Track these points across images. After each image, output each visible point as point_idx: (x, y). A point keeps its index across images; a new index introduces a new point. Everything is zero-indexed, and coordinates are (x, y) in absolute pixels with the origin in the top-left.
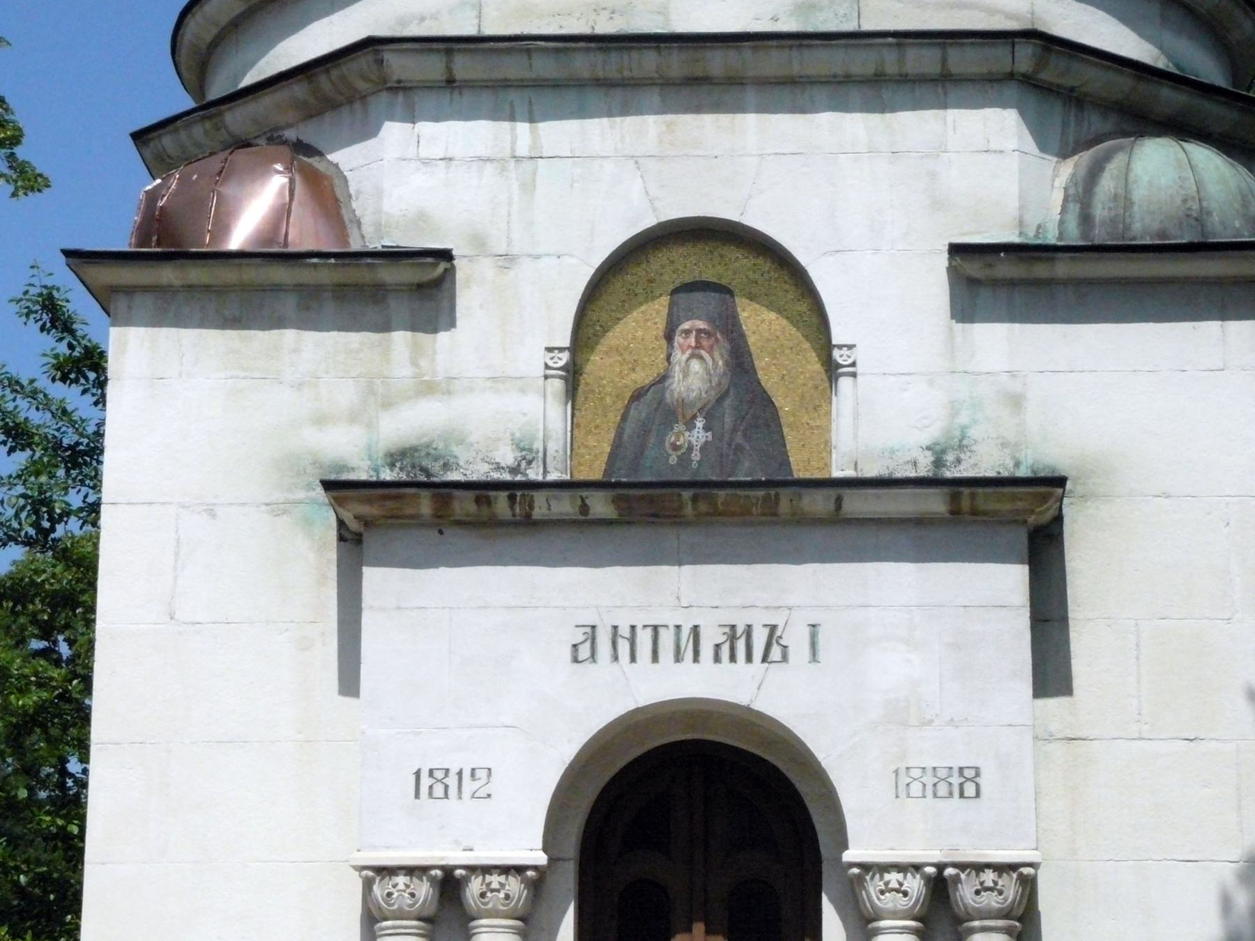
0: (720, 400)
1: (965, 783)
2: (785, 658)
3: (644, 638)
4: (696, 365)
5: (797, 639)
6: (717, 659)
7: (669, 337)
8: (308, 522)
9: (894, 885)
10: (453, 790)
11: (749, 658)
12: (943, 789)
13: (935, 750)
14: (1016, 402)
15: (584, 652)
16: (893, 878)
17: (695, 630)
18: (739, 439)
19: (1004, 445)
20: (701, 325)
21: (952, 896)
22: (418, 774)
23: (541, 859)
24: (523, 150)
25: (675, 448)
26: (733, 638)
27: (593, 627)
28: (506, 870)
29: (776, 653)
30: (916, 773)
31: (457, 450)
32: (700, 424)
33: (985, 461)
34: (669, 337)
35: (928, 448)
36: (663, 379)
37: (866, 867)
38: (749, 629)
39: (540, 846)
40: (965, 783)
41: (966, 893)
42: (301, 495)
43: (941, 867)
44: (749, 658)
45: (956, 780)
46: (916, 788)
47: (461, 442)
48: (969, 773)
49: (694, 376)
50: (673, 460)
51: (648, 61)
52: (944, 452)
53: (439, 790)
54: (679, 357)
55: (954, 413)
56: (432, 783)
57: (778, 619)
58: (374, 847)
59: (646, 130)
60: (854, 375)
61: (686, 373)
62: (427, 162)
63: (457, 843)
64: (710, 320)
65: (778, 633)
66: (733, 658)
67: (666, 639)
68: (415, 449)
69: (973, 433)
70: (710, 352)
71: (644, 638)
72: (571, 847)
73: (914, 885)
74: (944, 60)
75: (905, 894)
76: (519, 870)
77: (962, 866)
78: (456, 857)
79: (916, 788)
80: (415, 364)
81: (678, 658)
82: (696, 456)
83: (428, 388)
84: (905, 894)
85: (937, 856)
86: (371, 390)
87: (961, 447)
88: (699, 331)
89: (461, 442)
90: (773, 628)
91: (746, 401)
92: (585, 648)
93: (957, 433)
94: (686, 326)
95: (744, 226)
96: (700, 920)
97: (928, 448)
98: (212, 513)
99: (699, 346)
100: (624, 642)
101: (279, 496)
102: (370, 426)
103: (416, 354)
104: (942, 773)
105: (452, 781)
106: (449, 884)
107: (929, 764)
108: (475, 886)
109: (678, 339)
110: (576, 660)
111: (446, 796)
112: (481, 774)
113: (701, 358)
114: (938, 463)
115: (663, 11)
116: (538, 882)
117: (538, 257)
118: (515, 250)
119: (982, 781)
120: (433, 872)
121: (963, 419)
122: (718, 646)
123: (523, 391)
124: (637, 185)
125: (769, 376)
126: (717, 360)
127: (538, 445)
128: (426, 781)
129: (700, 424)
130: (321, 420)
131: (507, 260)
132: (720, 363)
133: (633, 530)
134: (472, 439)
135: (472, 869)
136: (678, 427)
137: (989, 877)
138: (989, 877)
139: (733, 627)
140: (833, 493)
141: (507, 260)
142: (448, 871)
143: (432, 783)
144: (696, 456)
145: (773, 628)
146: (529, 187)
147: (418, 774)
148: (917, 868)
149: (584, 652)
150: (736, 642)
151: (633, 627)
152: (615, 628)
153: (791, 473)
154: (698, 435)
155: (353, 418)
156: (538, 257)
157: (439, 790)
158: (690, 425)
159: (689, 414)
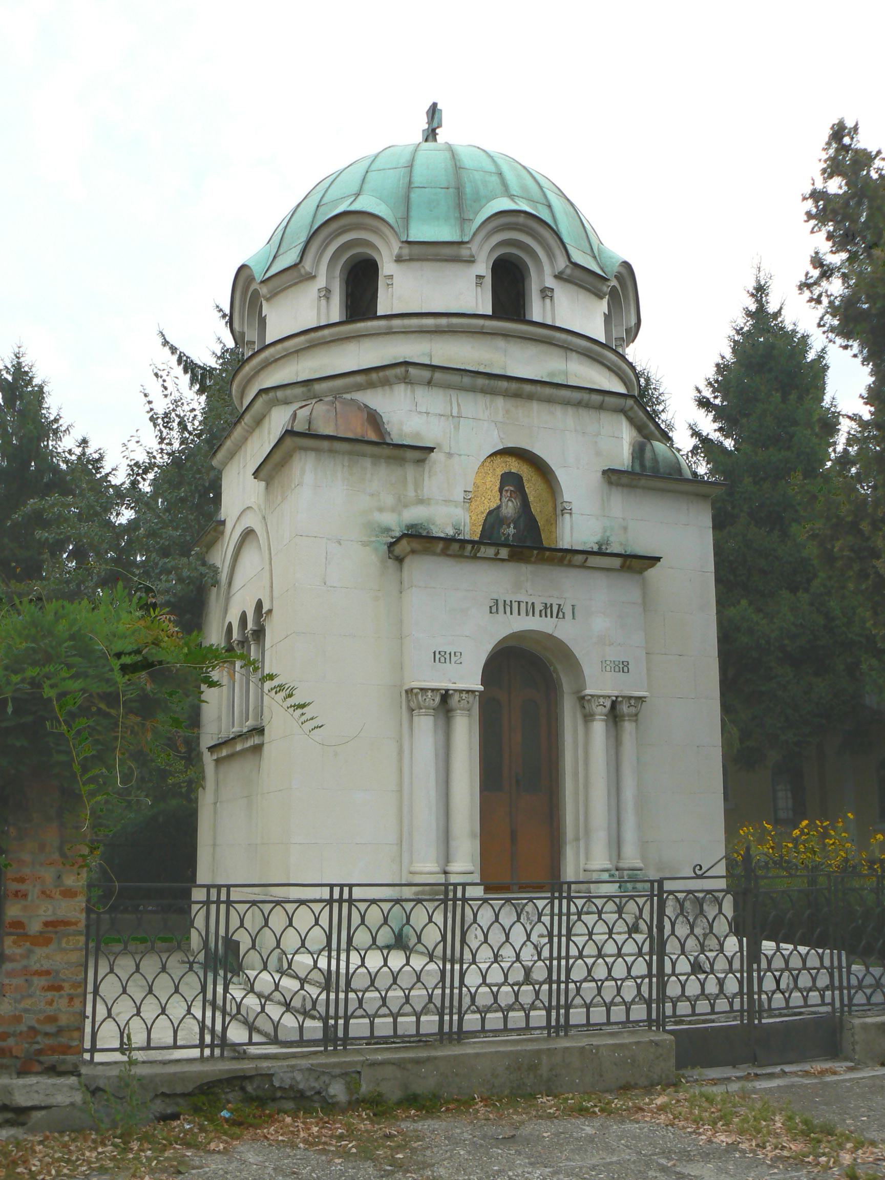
0: (519, 517)
1: (623, 667)
2: (564, 617)
3: (515, 605)
4: (510, 504)
5: (567, 610)
6: (541, 616)
7: (501, 490)
8: (376, 550)
11: (552, 617)
12: (617, 669)
13: (613, 654)
14: (625, 529)
15: (494, 609)
16: (601, 700)
17: (533, 604)
19: (621, 544)
20: (512, 488)
22: (435, 653)
26: (546, 608)
28: (468, 692)
29: (561, 615)
30: (608, 663)
31: (432, 527)
37: (592, 696)
38: (551, 605)
40: (623, 667)
42: (374, 539)
43: (617, 697)
44: (552, 617)
45: (621, 666)
46: (608, 668)
47: (433, 524)
48: (625, 664)
50: (503, 538)
51: (504, 384)
53: (442, 660)
54: (505, 500)
55: (605, 532)
56: (440, 657)
57: (561, 602)
58: (419, 681)
60: (571, 514)
62: (420, 413)
63: (450, 680)
64: (515, 487)
66: (546, 616)
67: (523, 606)
68: (416, 525)
69: (612, 539)
71: (515, 605)
78: (451, 686)
79: (608, 668)
80: (416, 491)
81: (527, 614)
82: (511, 538)
83: (421, 501)
85: (616, 693)
86: (399, 500)
87: (607, 544)
89: (433, 524)
90: (560, 605)
92: (494, 607)
94: (507, 488)
99: (511, 496)
100: (508, 606)
101: (365, 539)
102: (400, 514)
104: (617, 663)
105: (447, 656)
106: (446, 696)
107: (612, 659)
108: (456, 697)
109: (504, 493)
110: (491, 612)
112: (458, 654)
114: (600, 548)
115: (504, 368)
119: (630, 666)
121: (608, 534)
122: (541, 611)
123: (456, 506)
124: (496, 432)
125: (535, 509)
126: (517, 502)
127: (462, 528)
128: (438, 656)
130: (381, 510)
131: (450, 455)
133: (510, 563)
134: (438, 523)
135: (455, 690)
136: (505, 526)
137: (464, 695)
140: (585, 556)
141: (450, 455)
142: (447, 691)
143: (440, 657)
144: (511, 538)
145: (560, 605)
146: (457, 428)
147: (435, 653)
149: (494, 609)
150: (547, 610)
154: (511, 530)
155: (393, 510)
156: (460, 455)
157: (442, 660)
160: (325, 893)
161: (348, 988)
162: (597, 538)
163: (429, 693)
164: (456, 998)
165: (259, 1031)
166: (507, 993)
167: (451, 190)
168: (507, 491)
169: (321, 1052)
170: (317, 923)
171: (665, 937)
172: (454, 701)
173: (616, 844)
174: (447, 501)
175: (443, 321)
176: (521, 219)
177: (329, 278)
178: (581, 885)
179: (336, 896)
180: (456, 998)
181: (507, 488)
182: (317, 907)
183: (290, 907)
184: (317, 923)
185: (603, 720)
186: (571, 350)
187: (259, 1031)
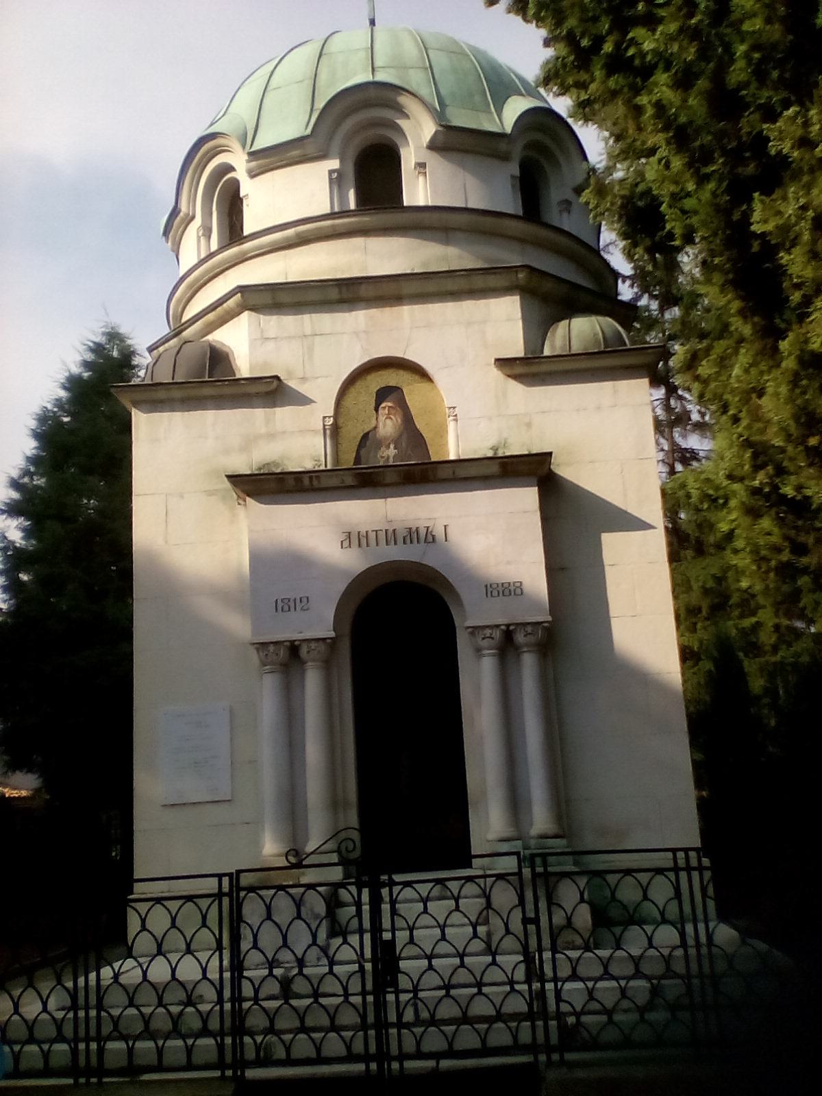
0: (401, 436)
4: (388, 421)
6: (405, 543)
7: (377, 409)
9: (488, 635)
10: (292, 609)
15: (346, 544)
16: (488, 632)
18: (409, 452)
21: (514, 638)
23: (332, 634)
24: (308, 331)
25: (382, 457)
27: (349, 533)
28: (318, 640)
32: (392, 446)
33: (516, 450)
34: (377, 409)
35: (491, 449)
36: (375, 428)
39: (332, 628)
41: (520, 638)
43: (508, 626)
49: (388, 425)
52: (497, 449)
53: (286, 608)
54: (382, 418)
59: (359, 318)
61: (385, 426)
64: (394, 402)
65: (430, 530)
68: (268, 464)
69: (509, 441)
70: (395, 415)
72: (347, 629)
73: (497, 634)
74: (691, 947)
75: (493, 638)
76: (324, 639)
77: (517, 624)
83: (271, 436)
84: (493, 638)
88: (389, 407)
91: (411, 435)
93: (503, 442)
95: (405, 359)
96: (542, 1053)
97: (491, 449)
98: (182, 497)
103: (268, 421)
106: (294, 649)
109: (380, 411)
111: (289, 610)
113: (390, 418)
116: (331, 644)
117: (317, 378)
118: (306, 376)
120: (285, 644)
122: (404, 538)
129: (392, 446)
132: (399, 420)
133: (363, 490)
138: (529, 629)
139: (410, 529)
142: (292, 642)
148: (498, 626)
151: (367, 532)
152: (359, 532)
153: (429, 457)
154: (392, 451)
157: (286, 608)
158: (388, 447)
159: (388, 443)
160: (665, 860)
161: (100, 1007)
162: (492, 442)
163: (272, 648)
164: (93, 1023)
165: (346, 1028)
166: (191, 1013)
167: (306, 82)
168: (384, 408)
169: (69, 1086)
170: (204, 925)
171: (130, 944)
172: (304, 651)
173: (516, 803)
174: (302, 432)
175: (290, 232)
176: (372, 93)
177: (207, 214)
178: (316, 862)
179: (681, 863)
180: (93, 1023)
181: (383, 405)
182: (204, 903)
183: (174, 905)
184: (204, 925)
185: (493, 655)
186: (454, 229)
187: (346, 1028)
